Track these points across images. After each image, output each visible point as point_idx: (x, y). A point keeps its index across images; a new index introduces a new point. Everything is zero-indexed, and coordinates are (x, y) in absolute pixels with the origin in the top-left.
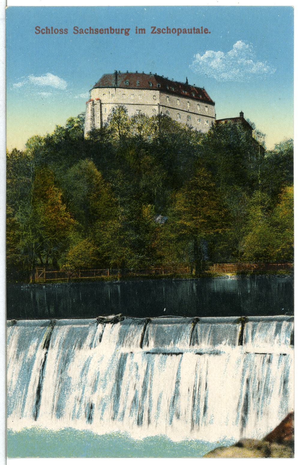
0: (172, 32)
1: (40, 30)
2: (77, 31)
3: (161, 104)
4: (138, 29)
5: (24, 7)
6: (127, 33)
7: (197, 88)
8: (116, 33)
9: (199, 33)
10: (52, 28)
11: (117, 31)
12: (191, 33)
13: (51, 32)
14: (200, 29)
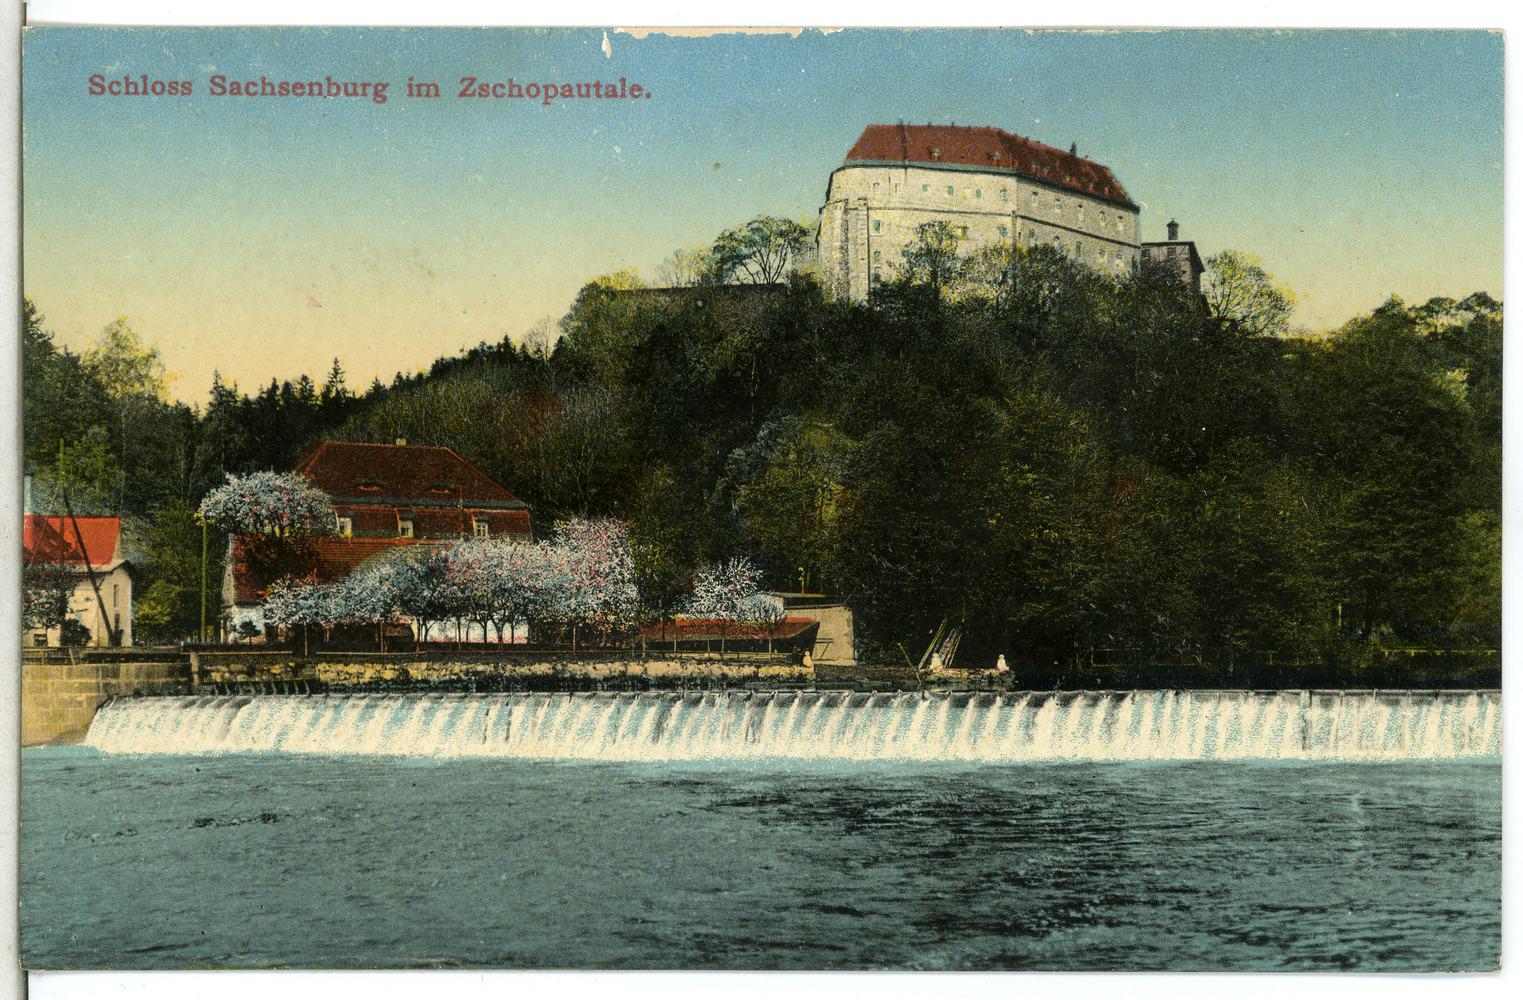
0: (154, 90)
1: (106, 85)
2: (224, 88)
3: (1018, 213)
4: (415, 83)
7: (1097, 166)
8: (580, 95)
10: (145, 78)
11: (584, 90)
12: (588, 95)
14: (619, 85)
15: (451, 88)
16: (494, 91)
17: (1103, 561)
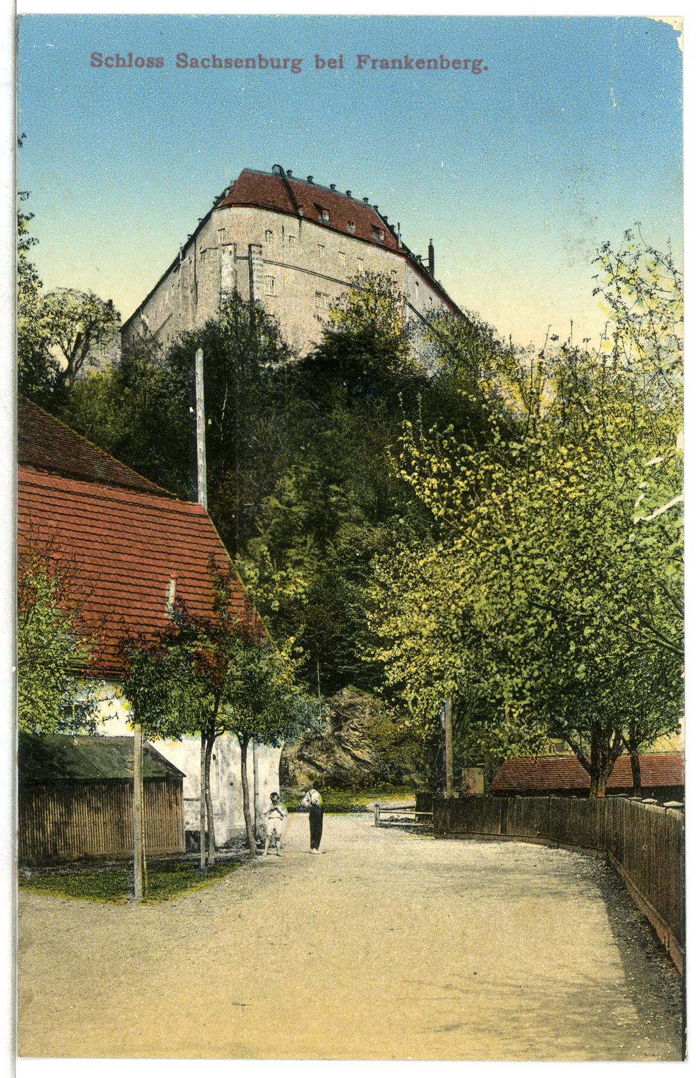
0: (143, 61)
1: (103, 60)
2: (186, 62)
8: (273, 67)
10: (130, 55)
16: (202, 62)
17: (600, 574)
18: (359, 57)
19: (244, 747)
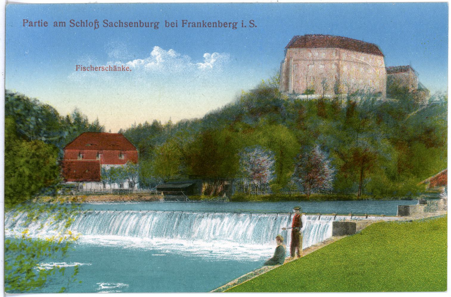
1: (75, 23)
5: (157, 4)
6: (234, 27)
9: (32, 26)
13: (85, 25)
15: (162, 25)
18: (183, 21)
19: (138, 182)
